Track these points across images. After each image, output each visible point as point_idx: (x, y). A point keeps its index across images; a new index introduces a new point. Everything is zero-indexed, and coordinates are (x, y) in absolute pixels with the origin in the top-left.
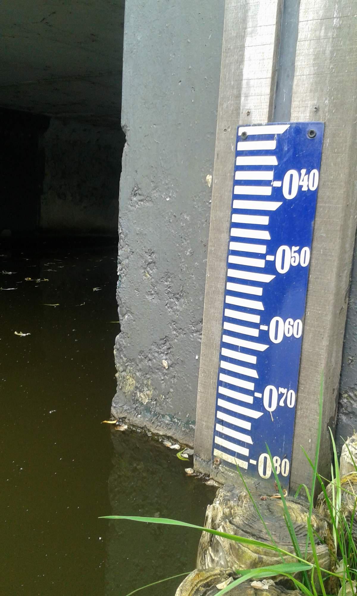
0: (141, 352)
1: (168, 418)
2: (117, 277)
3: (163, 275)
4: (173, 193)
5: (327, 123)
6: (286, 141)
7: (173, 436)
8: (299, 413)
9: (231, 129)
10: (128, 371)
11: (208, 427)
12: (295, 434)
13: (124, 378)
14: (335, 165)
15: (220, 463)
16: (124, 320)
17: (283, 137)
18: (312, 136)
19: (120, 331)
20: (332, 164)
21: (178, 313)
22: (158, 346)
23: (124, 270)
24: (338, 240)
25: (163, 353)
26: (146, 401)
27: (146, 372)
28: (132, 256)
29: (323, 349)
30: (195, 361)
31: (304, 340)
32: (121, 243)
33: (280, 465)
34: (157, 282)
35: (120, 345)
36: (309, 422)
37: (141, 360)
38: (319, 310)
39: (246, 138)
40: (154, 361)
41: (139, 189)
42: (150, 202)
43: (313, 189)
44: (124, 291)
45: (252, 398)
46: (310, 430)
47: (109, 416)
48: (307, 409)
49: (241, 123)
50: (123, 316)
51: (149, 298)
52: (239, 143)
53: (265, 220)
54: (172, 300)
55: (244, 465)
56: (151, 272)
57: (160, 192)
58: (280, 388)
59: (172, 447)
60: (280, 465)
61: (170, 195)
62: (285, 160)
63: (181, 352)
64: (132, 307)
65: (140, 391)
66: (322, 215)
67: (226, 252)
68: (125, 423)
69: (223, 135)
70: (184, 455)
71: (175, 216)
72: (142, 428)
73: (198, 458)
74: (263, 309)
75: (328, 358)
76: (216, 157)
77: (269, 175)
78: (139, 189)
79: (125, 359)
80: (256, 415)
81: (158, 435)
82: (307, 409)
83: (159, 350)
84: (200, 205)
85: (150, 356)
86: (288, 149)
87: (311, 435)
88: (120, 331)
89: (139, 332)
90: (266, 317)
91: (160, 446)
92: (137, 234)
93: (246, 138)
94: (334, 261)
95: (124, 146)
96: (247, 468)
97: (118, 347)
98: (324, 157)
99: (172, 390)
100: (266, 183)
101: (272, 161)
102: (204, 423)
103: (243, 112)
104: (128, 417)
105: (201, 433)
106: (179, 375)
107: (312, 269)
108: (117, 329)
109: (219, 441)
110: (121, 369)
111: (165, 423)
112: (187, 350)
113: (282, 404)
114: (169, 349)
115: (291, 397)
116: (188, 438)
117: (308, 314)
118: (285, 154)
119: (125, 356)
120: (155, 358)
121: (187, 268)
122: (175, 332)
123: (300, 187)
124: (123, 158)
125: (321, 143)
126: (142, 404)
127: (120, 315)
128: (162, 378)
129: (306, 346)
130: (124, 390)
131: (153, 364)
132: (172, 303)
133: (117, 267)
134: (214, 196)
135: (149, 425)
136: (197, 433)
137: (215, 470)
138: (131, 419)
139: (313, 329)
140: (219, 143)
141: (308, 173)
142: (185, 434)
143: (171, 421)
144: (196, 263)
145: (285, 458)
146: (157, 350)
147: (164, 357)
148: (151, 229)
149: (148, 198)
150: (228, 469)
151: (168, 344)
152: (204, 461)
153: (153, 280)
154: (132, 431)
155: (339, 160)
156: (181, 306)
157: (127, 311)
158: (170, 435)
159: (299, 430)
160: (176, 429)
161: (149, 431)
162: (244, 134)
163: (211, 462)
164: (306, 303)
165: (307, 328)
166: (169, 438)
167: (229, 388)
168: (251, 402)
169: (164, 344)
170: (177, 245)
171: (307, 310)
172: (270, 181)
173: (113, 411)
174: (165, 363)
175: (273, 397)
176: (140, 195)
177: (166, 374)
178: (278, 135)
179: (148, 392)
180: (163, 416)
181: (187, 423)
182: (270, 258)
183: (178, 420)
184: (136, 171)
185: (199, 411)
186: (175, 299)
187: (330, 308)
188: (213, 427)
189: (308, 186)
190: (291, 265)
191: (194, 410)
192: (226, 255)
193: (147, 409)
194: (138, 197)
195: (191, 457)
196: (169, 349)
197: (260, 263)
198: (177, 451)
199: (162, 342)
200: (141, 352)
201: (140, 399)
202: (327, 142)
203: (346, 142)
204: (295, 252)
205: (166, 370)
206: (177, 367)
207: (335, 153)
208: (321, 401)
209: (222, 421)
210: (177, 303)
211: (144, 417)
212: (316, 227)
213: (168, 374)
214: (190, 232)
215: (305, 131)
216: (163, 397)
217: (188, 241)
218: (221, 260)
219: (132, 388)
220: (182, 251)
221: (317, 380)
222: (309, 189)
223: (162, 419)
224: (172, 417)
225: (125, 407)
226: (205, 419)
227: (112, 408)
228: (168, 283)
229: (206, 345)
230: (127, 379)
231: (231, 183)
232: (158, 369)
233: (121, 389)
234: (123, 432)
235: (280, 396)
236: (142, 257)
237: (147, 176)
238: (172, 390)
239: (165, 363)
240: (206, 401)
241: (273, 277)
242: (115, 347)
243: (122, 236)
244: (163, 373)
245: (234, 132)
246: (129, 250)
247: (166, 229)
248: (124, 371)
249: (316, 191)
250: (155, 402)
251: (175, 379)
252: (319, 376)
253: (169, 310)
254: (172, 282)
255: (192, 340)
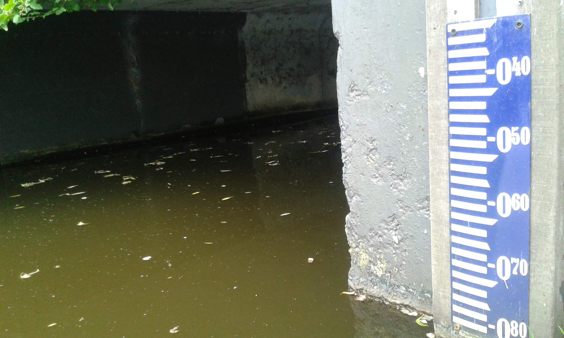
0: (371, 230)
1: (404, 288)
2: (342, 165)
3: (385, 159)
4: (387, 86)
5: (532, 15)
6: (495, 33)
7: (410, 305)
8: (532, 280)
9: (441, 27)
10: (360, 247)
11: (445, 297)
12: (530, 299)
13: (357, 253)
14: (545, 50)
15: (460, 329)
16: (352, 202)
17: (492, 31)
18: (520, 27)
19: (349, 211)
20: (542, 50)
21: (403, 192)
22: (387, 223)
23: (348, 157)
24: (556, 119)
25: (392, 229)
26: (380, 273)
27: (378, 247)
28: (354, 145)
29: (551, 220)
30: (424, 235)
31: (532, 213)
32: (343, 134)
33: (518, 329)
34: (380, 166)
35: (350, 224)
36: (542, 288)
37: (372, 237)
38: (544, 184)
39: (455, 33)
40: (385, 237)
41: (355, 85)
42: (367, 96)
43: (526, 73)
44: (349, 176)
45: (486, 268)
46: (544, 295)
47: (347, 288)
48: (540, 276)
49: (449, 21)
50: (351, 198)
51: (374, 181)
52: (449, 39)
53: (482, 105)
54: (396, 181)
55: (484, 330)
56: (373, 157)
57: (375, 86)
58: (512, 258)
59: (410, 314)
60: (518, 329)
61: (385, 87)
62: (496, 50)
63: (409, 227)
64: (359, 190)
65: (374, 265)
66: (538, 96)
67: (447, 136)
68: (363, 294)
69: (433, 33)
70: (422, 321)
71: (392, 106)
72: (380, 298)
73: (438, 325)
74: (489, 187)
75: (556, 227)
76: (428, 52)
77: (482, 65)
78: (355, 85)
79: (357, 236)
80: (491, 284)
81: (395, 304)
82: (540, 276)
83: (389, 227)
84: (414, 94)
85: (380, 232)
86: (498, 40)
87: (546, 300)
88: (349, 211)
89: (367, 212)
90: (492, 193)
91: (398, 312)
92: (358, 125)
93: (455, 33)
94: (554, 138)
95: (338, 50)
96: (486, 332)
97: (349, 226)
98: (533, 45)
99: (404, 263)
100: (481, 72)
101: (484, 52)
102: (441, 293)
103: (450, 10)
104: (365, 288)
105: (439, 302)
106: (410, 248)
107: (534, 146)
108: (346, 209)
109: (456, 308)
110: (354, 245)
111: (401, 293)
112: (415, 226)
113: (515, 273)
114: (398, 225)
115: (522, 266)
116: (424, 306)
117: (533, 188)
118: (496, 45)
119: (356, 234)
120: (385, 234)
121: (408, 151)
122: (401, 210)
123: (514, 73)
124: (338, 60)
125: (528, 32)
126: (377, 276)
127: (348, 198)
128: (394, 252)
129: (534, 218)
130: (359, 264)
131: (384, 239)
132: (397, 183)
133: (341, 155)
134: (430, 87)
135: (386, 295)
136: (435, 302)
137: (456, 335)
138: (368, 290)
139: (539, 202)
140: (430, 40)
141: (519, 60)
142: (421, 302)
143: (407, 291)
144: (416, 147)
145: (523, 321)
146: (386, 227)
147: (394, 233)
148: (369, 119)
149: (364, 93)
150: (468, 334)
151: (396, 221)
152: (445, 327)
153: (376, 164)
154: (371, 301)
155: (548, 46)
156: (405, 186)
157: (355, 193)
158: (406, 303)
159: (533, 295)
160: (412, 299)
161: (386, 300)
162: (453, 31)
163: (451, 328)
164: (531, 178)
165: (534, 201)
166: (406, 306)
167: (463, 261)
168: (486, 273)
169: (392, 221)
170: (397, 132)
171: (532, 184)
172: (484, 70)
173: (350, 283)
174: (395, 239)
175: (506, 267)
176: (356, 90)
177: (397, 248)
178: (487, 29)
179: (382, 265)
180: (399, 287)
181: (423, 292)
182: (491, 139)
183: (413, 289)
184: (351, 71)
185: (434, 282)
186: (399, 181)
187: (554, 181)
188: (450, 296)
189: (521, 71)
190: (512, 144)
191: (429, 280)
192: (447, 139)
193: (383, 280)
194: (355, 93)
195: (430, 323)
196: (398, 225)
197: (482, 145)
198: (416, 318)
199: (390, 219)
200: (371, 230)
201: (375, 272)
202: (534, 31)
203: (553, 30)
204: (515, 132)
205: (397, 244)
206: (407, 242)
207: (543, 40)
208: (553, 268)
209: (459, 291)
210: (401, 183)
211: (381, 288)
212: (533, 108)
213: (400, 248)
214: (407, 119)
215: (512, 23)
216: (397, 269)
217: (407, 127)
218: (442, 144)
219: (366, 263)
220: (402, 137)
221: (547, 249)
222: (522, 75)
223: (398, 290)
224: (407, 288)
225: (362, 280)
226: (442, 289)
227: (349, 281)
228: (391, 166)
229: (435, 222)
230: (360, 255)
231: (446, 74)
232: (389, 244)
233: (356, 263)
234: (363, 302)
235: (513, 265)
236: (364, 145)
237: (362, 73)
238: (404, 263)
239: (395, 239)
240: (441, 273)
241: (496, 156)
242: (346, 226)
243: (343, 128)
244: (394, 248)
245: (444, 30)
246: (351, 140)
247: (384, 118)
248: (357, 247)
249: (530, 75)
250: (389, 275)
251: (407, 253)
252: (549, 245)
253: (394, 190)
254: (395, 165)
255: (419, 216)
